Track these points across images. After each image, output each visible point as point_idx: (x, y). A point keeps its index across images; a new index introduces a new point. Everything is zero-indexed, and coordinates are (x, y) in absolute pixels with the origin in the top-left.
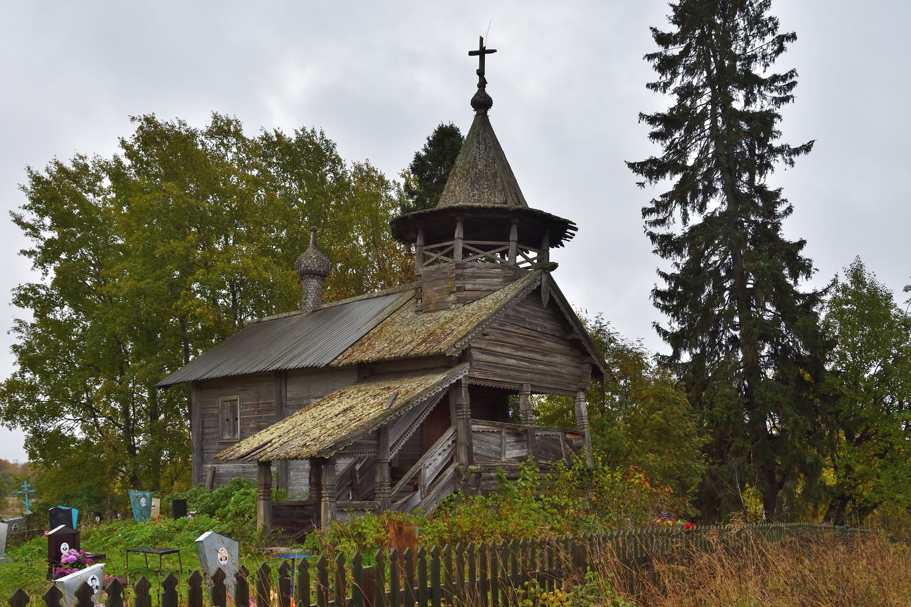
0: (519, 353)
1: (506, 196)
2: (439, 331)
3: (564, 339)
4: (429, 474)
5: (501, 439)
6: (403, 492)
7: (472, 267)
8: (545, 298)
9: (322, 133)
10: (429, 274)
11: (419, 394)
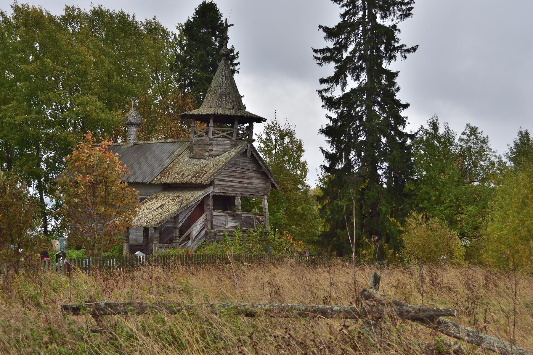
0: (236, 180)
1: (234, 105)
3: (258, 171)
4: (194, 233)
6: (184, 240)
7: (216, 140)
9: (133, 17)
10: (197, 141)
11: (192, 201)
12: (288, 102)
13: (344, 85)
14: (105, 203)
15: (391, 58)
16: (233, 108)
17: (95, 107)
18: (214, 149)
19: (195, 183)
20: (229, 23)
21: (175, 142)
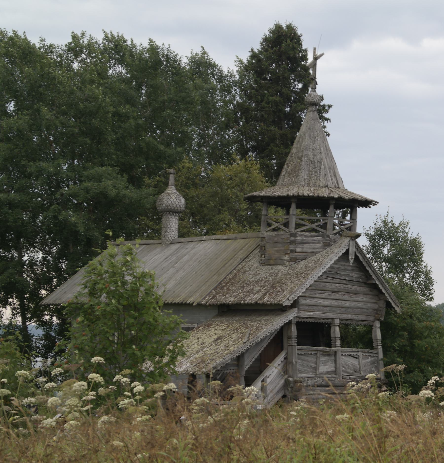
3: (365, 283)
5: (317, 359)
7: (302, 235)
17: (114, 184)
18: (298, 250)
21: (236, 239)
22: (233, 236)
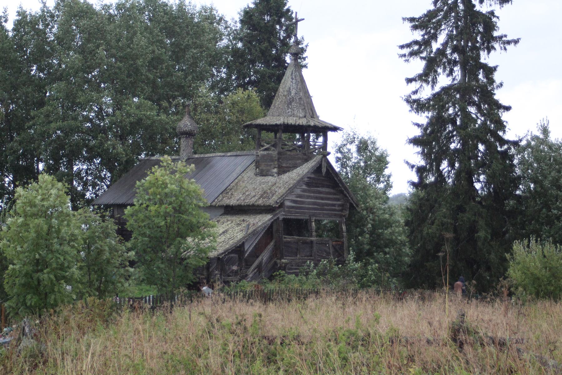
1: (306, 112)
2: (269, 191)
8: (324, 170)
10: (263, 156)
11: (260, 226)
12: (364, 93)
13: (434, 82)
14: (280, 280)
15: (489, 49)
16: (305, 117)
19: (262, 205)
20: (299, 17)
22: (235, 153)
